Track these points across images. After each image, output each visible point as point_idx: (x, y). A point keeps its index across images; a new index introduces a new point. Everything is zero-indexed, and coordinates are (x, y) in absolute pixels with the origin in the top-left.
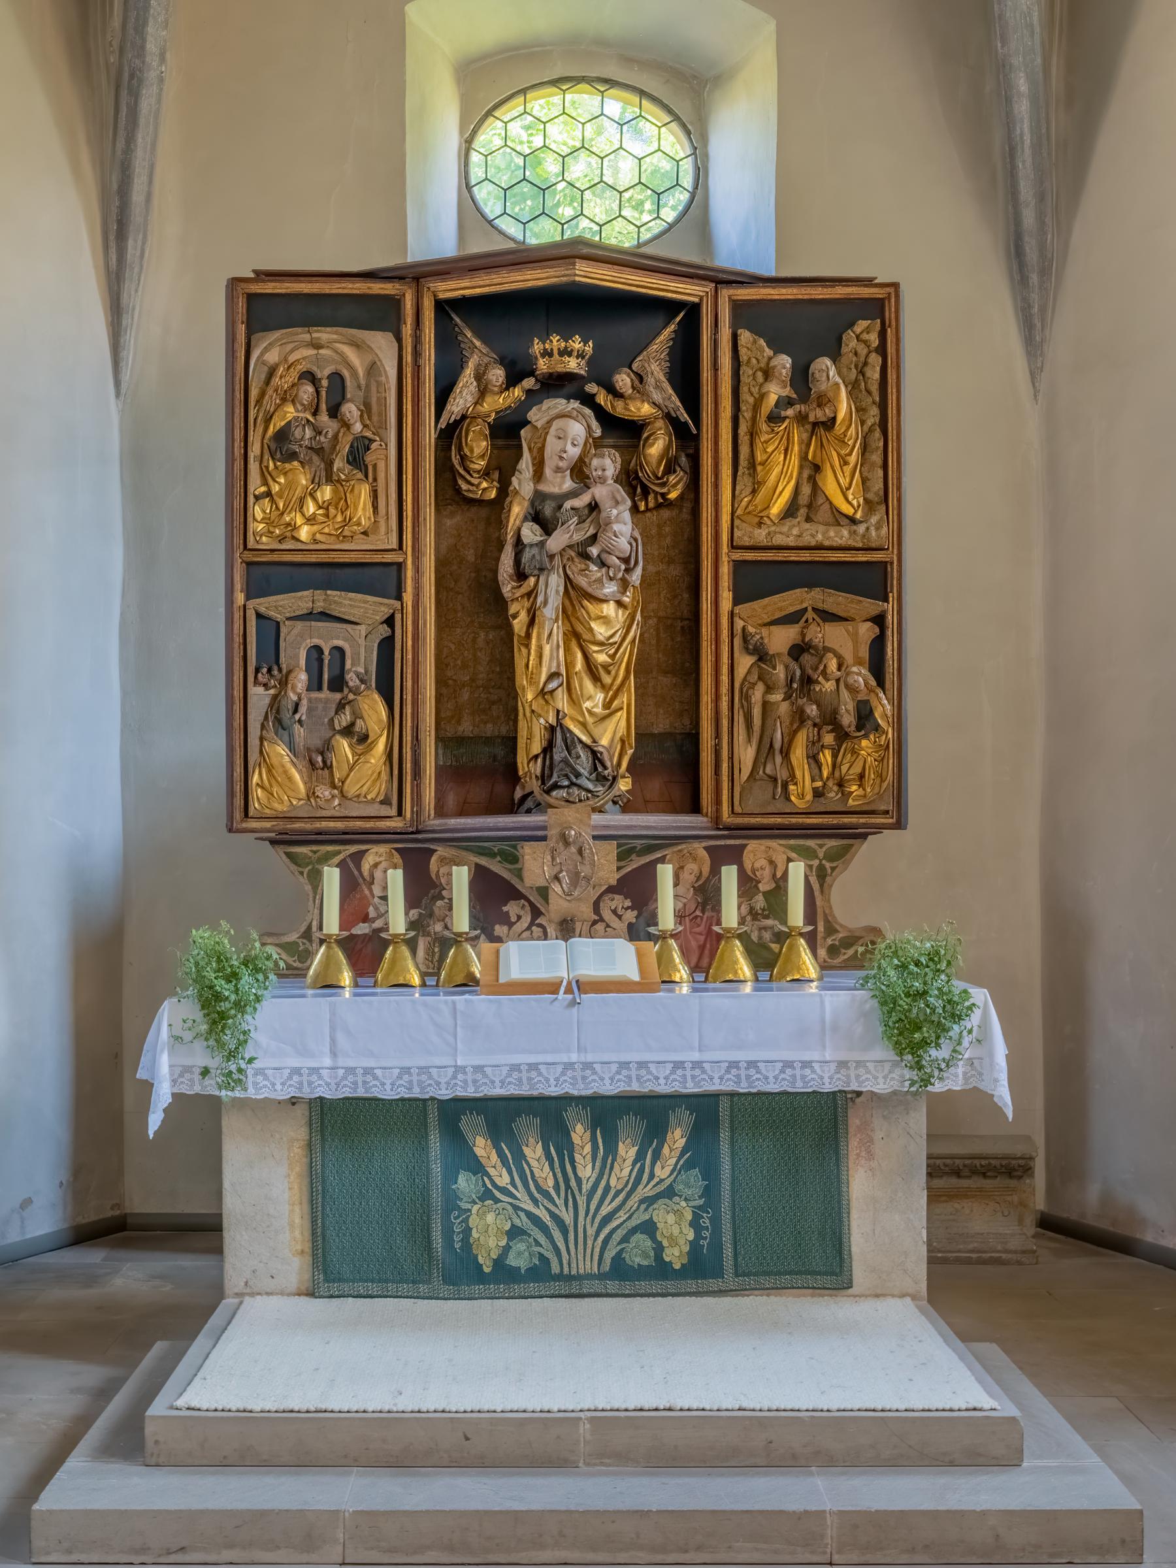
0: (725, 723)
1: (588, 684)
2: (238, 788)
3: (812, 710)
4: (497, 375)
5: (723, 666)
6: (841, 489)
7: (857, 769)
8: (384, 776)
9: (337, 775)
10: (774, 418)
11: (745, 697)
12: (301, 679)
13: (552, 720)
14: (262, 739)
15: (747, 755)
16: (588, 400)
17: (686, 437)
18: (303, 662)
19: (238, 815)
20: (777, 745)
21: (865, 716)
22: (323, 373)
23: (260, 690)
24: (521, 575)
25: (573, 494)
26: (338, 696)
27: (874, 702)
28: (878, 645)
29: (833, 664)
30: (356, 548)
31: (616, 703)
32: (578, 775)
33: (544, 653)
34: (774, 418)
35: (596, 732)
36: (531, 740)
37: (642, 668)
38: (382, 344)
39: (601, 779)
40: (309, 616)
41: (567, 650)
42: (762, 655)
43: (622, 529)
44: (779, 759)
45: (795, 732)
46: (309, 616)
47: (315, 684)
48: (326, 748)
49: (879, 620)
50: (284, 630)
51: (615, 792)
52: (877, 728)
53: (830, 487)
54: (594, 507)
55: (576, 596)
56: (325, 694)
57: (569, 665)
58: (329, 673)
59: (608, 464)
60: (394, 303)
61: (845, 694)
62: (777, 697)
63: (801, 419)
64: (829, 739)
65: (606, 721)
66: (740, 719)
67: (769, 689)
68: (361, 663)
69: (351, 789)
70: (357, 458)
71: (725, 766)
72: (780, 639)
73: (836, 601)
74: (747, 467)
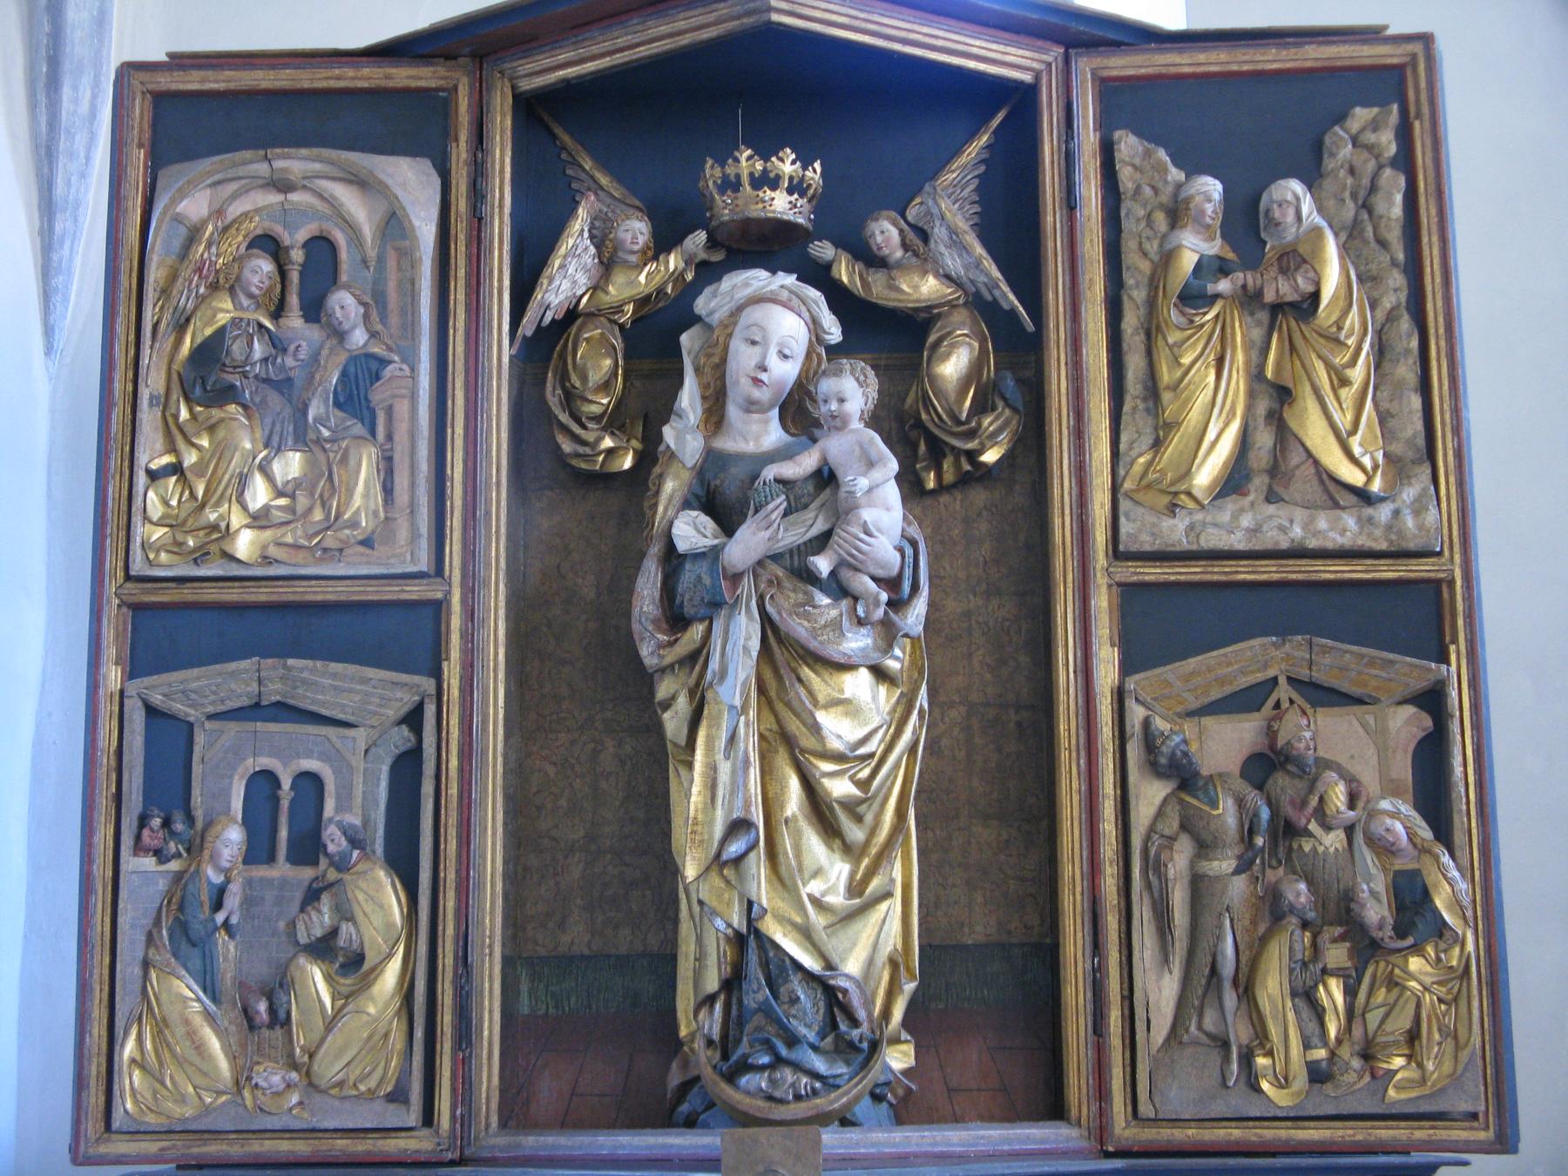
0: (1112, 922)
1: (814, 843)
2: (95, 1067)
3: (1299, 892)
4: (636, 230)
5: (1106, 803)
6: (1341, 435)
7: (1401, 1022)
8: (397, 1040)
9: (300, 1039)
10: (1193, 298)
11: (1155, 866)
12: (233, 837)
13: (737, 920)
14: (146, 965)
15: (1161, 991)
16: (818, 275)
17: (1017, 347)
18: (237, 804)
19: (92, 1126)
20: (1228, 968)
21: (1412, 901)
22: (295, 239)
23: (148, 863)
24: (676, 620)
25: (782, 454)
26: (307, 873)
27: (1432, 876)
28: (1432, 755)
29: (1338, 796)
30: (349, 573)
31: (875, 884)
32: (793, 1041)
33: (714, 783)
34: (1193, 298)
35: (833, 946)
36: (701, 964)
37: (935, 801)
38: (412, 183)
39: (844, 1049)
40: (255, 710)
41: (766, 772)
42: (1184, 776)
43: (882, 515)
44: (1230, 999)
45: (1264, 940)
46: (255, 710)
47: (259, 850)
48: (278, 986)
49: (1432, 700)
50: (200, 739)
51: (875, 1074)
52: (1440, 929)
53: (1315, 433)
54: (825, 478)
55: (784, 656)
56: (282, 869)
57: (771, 806)
58: (289, 824)
59: (852, 392)
60: (436, 105)
61: (1368, 857)
62: (1222, 865)
63: (1249, 299)
64: (1337, 955)
65: (853, 920)
66: (1143, 912)
67: (1204, 848)
68: (357, 801)
69: (329, 1068)
70: (356, 395)
71: (1115, 1016)
72: (1224, 744)
73: (1338, 661)
74: (1143, 397)
